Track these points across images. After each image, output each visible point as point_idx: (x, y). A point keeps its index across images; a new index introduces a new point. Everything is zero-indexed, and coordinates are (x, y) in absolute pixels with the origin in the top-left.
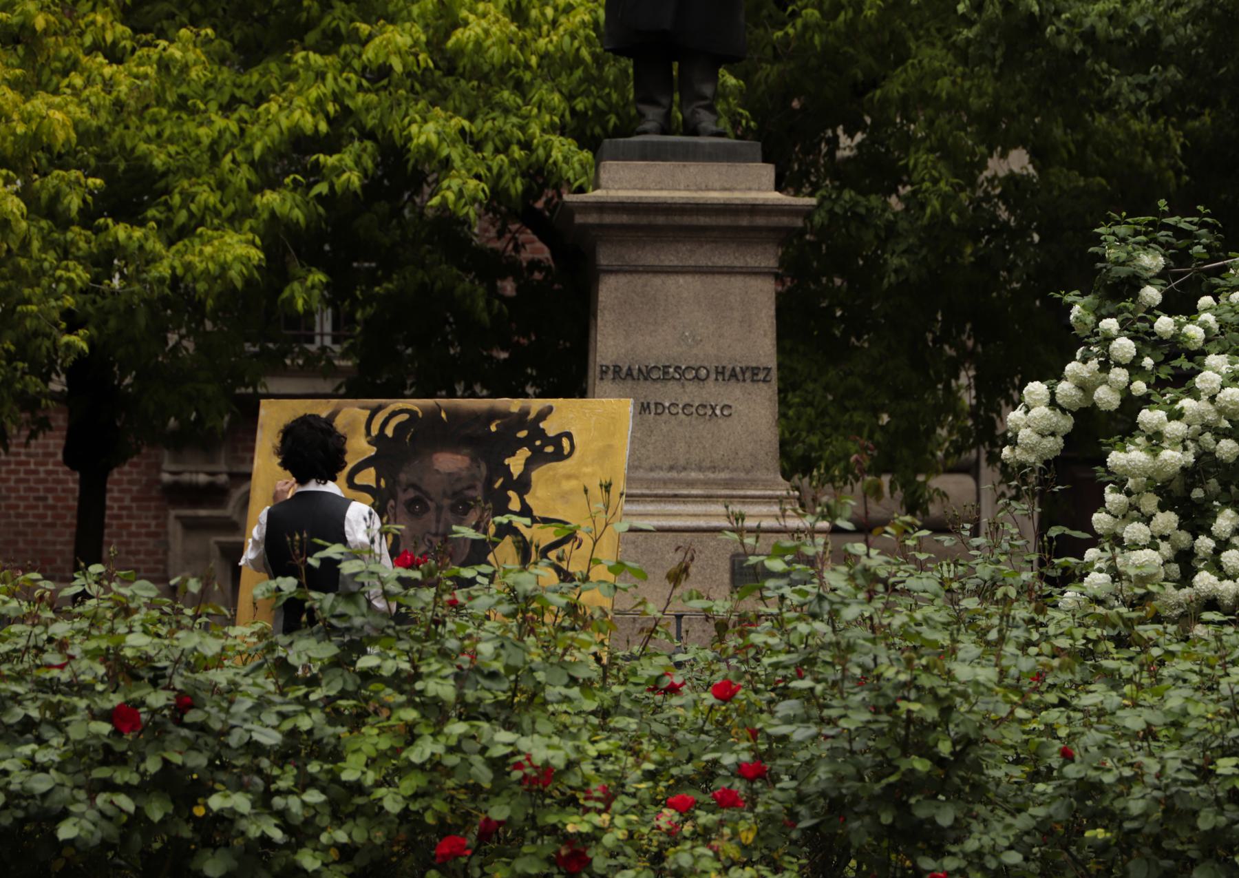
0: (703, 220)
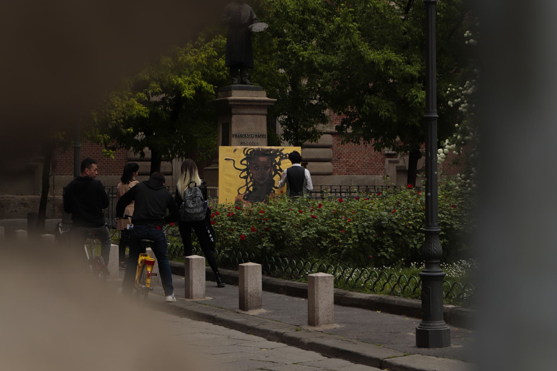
0: (254, 104)
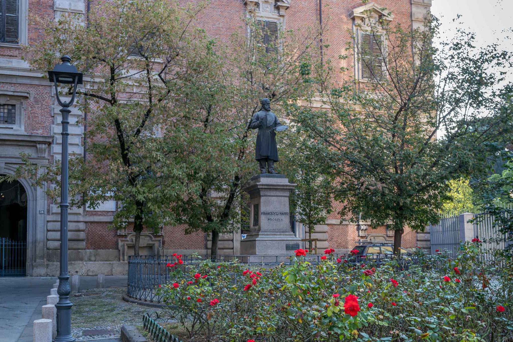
0: (279, 187)
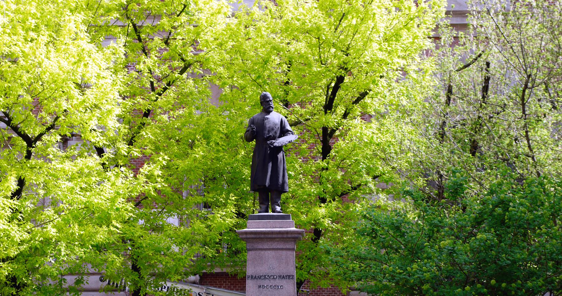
0: (274, 236)
